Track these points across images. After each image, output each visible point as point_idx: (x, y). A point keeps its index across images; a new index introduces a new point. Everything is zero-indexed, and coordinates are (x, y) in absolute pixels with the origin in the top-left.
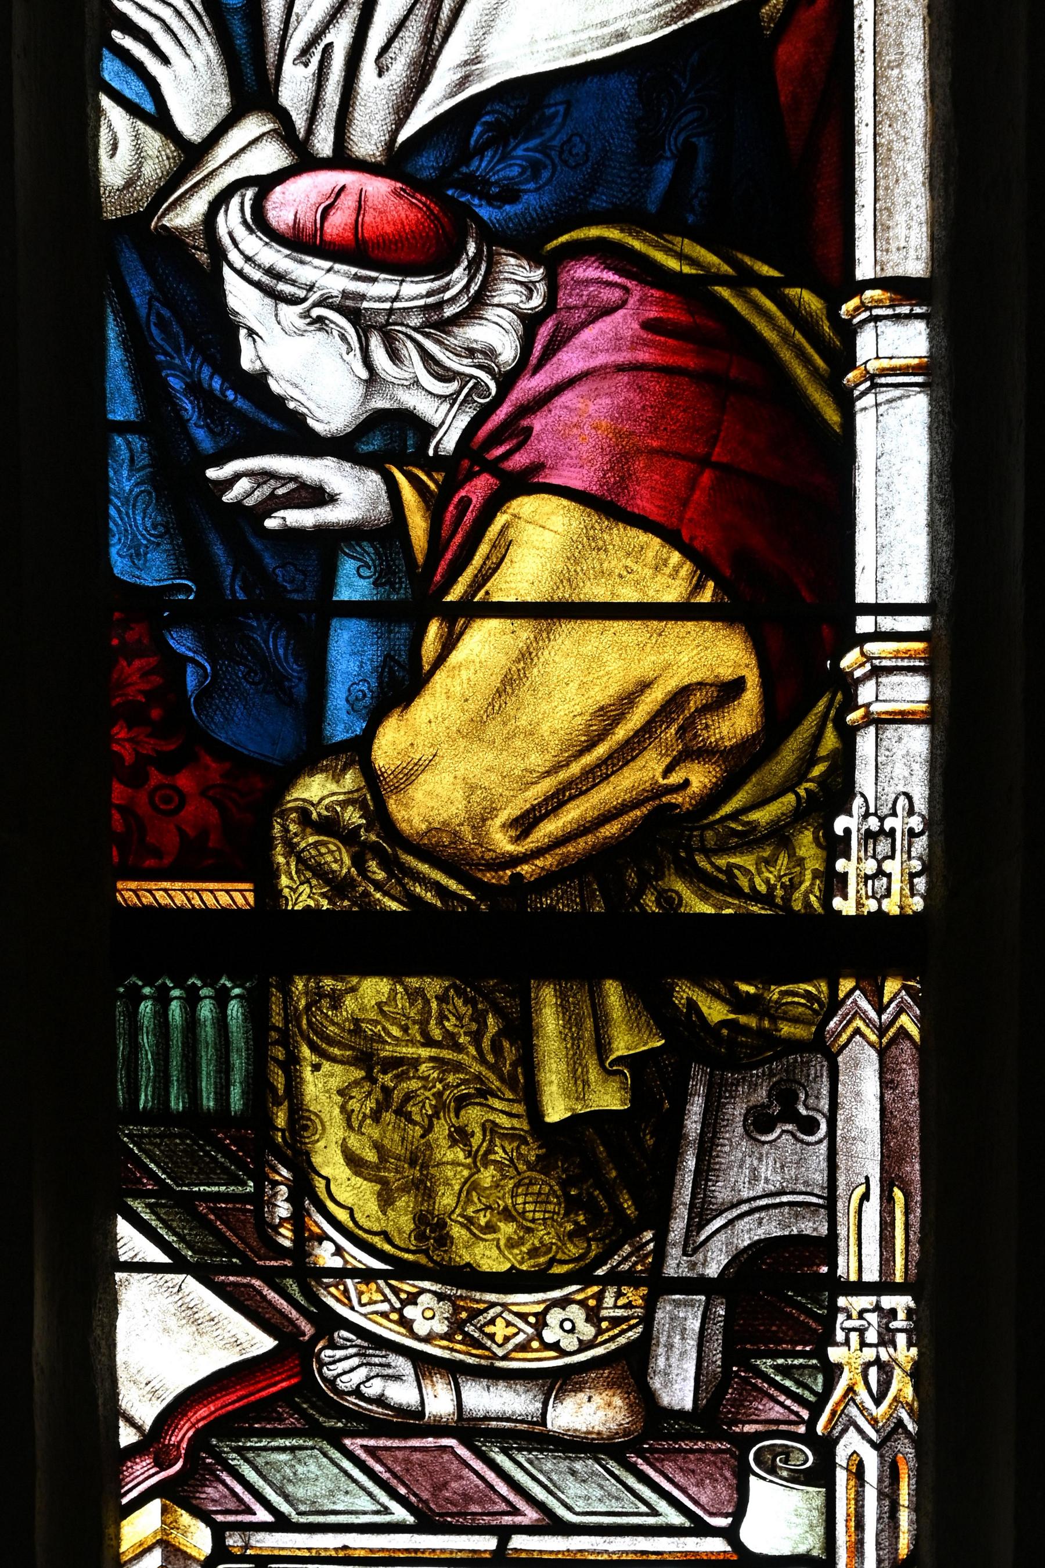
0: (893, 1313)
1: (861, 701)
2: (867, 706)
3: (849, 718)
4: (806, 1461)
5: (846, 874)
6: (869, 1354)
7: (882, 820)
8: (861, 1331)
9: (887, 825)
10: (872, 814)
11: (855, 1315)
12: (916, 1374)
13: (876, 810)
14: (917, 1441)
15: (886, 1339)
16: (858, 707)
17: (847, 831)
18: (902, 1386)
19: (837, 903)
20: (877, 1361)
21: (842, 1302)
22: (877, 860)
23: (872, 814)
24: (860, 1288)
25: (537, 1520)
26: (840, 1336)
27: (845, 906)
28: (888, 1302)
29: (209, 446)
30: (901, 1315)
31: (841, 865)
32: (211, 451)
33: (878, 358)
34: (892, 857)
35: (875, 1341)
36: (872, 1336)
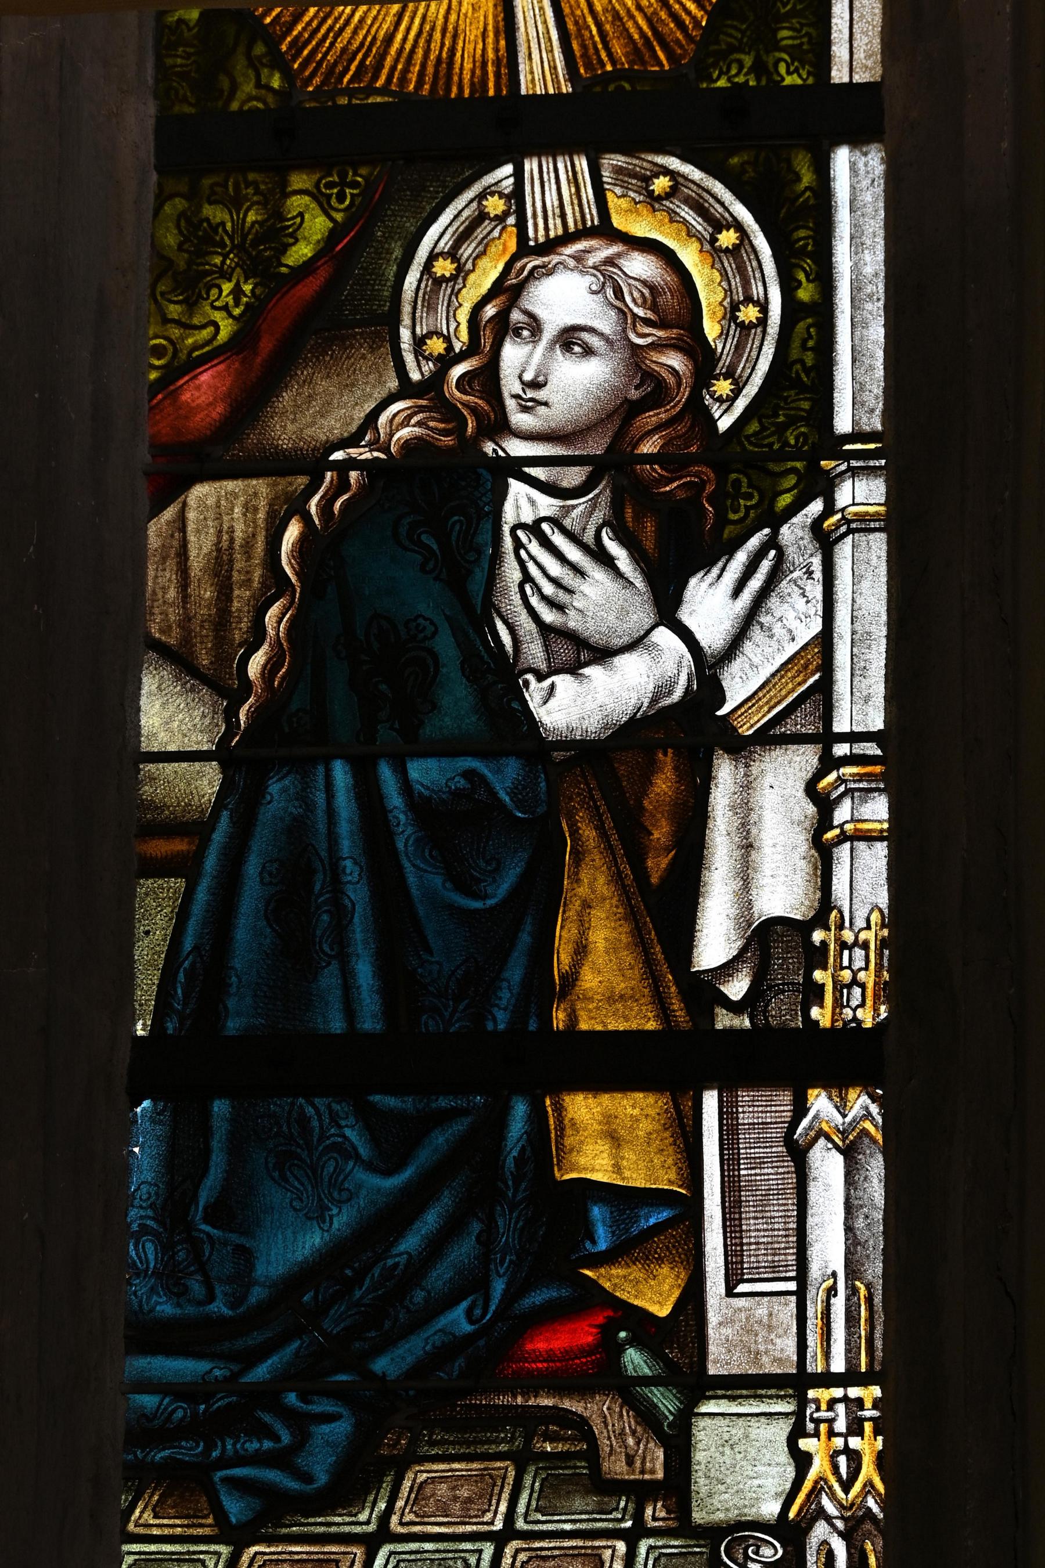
0: (859, 1402)
1: (836, 823)
2: (843, 510)
3: (825, 525)
4: (776, 1552)
5: (823, 985)
6: (838, 1442)
7: (854, 1010)
8: (831, 1421)
9: (862, 936)
10: (846, 968)
11: (824, 1406)
12: (881, 1460)
13: (850, 964)
14: (883, 1528)
15: (855, 1428)
16: (832, 828)
17: (824, 943)
18: (868, 1470)
19: (815, 1012)
20: (847, 1450)
21: (811, 1394)
22: (852, 971)
23: (846, 968)
24: (828, 1379)
25: (169, 246)
26: (810, 1426)
27: (821, 1015)
28: (854, 1392)
29: (338, 1024)
30: (868, 1404)
31: (818, 975)
32: (339, 1032)
33: (854, 504)
34: (866, 968)
35: (844, 1430)
36: (841, 1426)
